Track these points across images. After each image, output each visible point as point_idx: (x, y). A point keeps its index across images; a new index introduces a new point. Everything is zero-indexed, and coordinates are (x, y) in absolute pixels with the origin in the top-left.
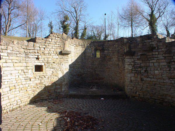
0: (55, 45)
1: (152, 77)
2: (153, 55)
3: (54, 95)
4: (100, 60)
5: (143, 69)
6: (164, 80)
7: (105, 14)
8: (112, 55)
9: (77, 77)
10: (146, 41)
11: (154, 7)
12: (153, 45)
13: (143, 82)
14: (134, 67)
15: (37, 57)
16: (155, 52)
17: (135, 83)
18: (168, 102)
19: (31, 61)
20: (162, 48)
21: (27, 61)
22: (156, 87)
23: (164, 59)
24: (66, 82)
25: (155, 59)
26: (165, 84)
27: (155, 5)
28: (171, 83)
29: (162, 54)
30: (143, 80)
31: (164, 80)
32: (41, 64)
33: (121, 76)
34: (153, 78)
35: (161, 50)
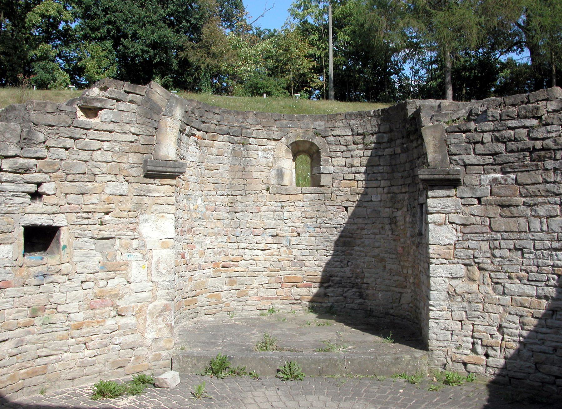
15: (32, 188)
24: (160, 303)
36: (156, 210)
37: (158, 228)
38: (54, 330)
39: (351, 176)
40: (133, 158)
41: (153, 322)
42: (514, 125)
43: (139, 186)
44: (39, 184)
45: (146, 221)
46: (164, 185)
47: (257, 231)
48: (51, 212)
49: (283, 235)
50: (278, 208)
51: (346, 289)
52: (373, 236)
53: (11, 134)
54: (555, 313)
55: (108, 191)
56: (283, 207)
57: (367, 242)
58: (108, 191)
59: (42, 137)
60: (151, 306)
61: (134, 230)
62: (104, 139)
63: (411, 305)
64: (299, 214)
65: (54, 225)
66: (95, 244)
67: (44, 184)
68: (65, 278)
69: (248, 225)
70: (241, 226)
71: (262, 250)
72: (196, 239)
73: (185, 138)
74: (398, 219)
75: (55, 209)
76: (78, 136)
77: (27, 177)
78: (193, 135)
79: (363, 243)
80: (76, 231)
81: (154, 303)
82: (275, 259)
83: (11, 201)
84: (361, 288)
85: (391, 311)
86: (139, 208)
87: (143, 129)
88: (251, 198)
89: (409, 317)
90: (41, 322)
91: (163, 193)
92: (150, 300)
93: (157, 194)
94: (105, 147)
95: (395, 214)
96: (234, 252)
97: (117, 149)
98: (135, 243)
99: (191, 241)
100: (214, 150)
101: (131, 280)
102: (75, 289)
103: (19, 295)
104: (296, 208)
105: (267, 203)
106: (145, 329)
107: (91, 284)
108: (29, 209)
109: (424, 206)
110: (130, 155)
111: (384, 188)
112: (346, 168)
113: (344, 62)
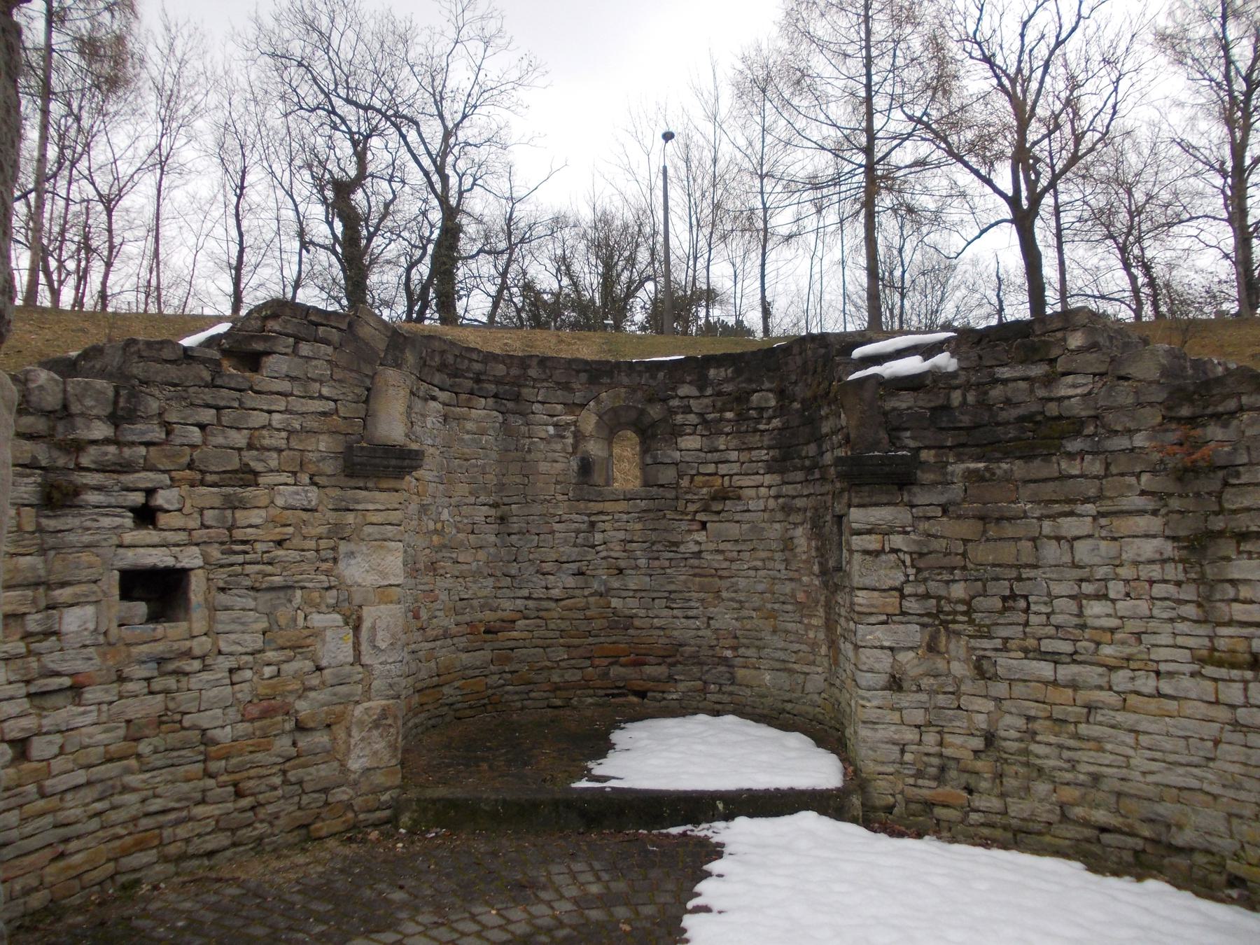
0: (297, 404)
1: (1066, 647)
2: (1063, 477)
3: (277, 816)
4: (643, 504)
5: (993, 588)
6: (1158, 673)
7: (668, 136)
8: (735, 468)
9: (462, 642)
10: (1004, 372)
11: (1034, 86)
12: (1060, 399)
13: (1000, 689)
14: (919, 570)
15: (138, 498)
16: (1082, 454)
17: (932, 692)
18: (1208, 852)
19: (86, 538)
20: (1132, 425)
21: (51, 541)
22: (1096, 731)
23: (1155, 513)
24: (377, 704)
25: (1080, 508)
26: (1173, 705)
27: (1039, 73)
28: (1217, 702)
29: (1138, 476)
30: (995, 677)
31: (1158, 673)
32: (170, 562)
33: (811, 634)
34: (1073, 658)
35: (1124, 443)
36: (369, 535)
37: (373, 567)
38: (175, 761)
39: (711, 468)
40: (324, 444)
41: (362, 739)
42: (1006, 376)
43: (338, 492)
44: (150, 492)
45: (351, 554)
46: (382, 490)
47: (547, 567)
48: (172, 541)
49: (594, 573)
50: (584, 527)
51: (706, 668)
52: (752, 573)
53: (97, 400)
54: (1093, 711)
55: (280, 502)
56: (592, 524)
57: (742, 583)
58: (280, 502)
59: (154, 406)
60: (358, 711)
61: (328, 573)
62: (273, 408)
63: (823, 695)
64: (621, 535)
65: (179, 565)
66: (255, 599)
67: (161, 491)
68: (197, 665)
69: (531, 557)
70: (520, 559)
71: (557, 600)
72: (440, 583)
73: (418, 404)
74: (796, 541)
75: (182, 537)
76: (222, 404)
77: (128, 479)
78: (434, 398)
79: (734, 584)
80: (221, 576)
81: (366, 705)
82: (580, 615)
83: (95, 525)
84: (732, 666)
85: (789, 706)
86: (338, 533)
87: (344, 390)
88: (537, 509)
89: (821, 717)
90: (151, 748)
91: (382, 504)
92: (357, 698)
93: (371, 507)
94: (274, 424)
95: (791, 533)
96: (507, 604)
97: (298, 427)
98: (331, 597)
99: (431, 587)
100: (470, 426)
101: (324, 663)
102: (217, 684)
103: (110, 698)
104: (616, 525)
105: (565, 517)
106: (349, 750)
107: (248, 674)
108: (128, 538)
109: (845, 520)
110: (321, 437)
111: (769, 487)
112: (703, 455)
113: (53, 436)
